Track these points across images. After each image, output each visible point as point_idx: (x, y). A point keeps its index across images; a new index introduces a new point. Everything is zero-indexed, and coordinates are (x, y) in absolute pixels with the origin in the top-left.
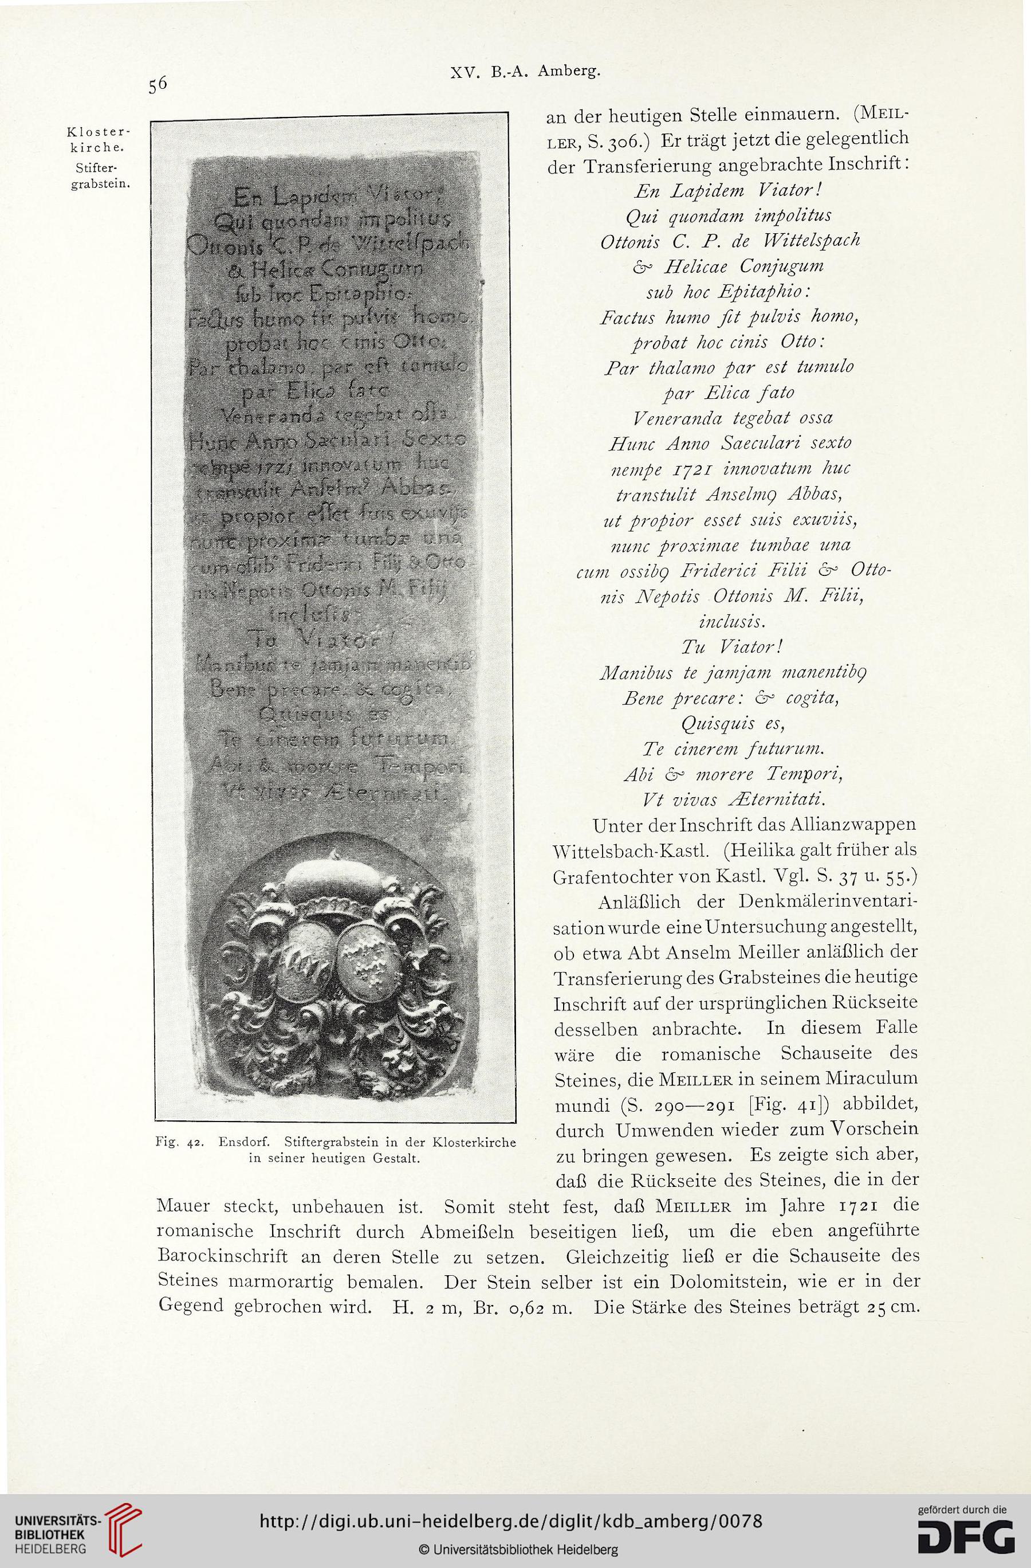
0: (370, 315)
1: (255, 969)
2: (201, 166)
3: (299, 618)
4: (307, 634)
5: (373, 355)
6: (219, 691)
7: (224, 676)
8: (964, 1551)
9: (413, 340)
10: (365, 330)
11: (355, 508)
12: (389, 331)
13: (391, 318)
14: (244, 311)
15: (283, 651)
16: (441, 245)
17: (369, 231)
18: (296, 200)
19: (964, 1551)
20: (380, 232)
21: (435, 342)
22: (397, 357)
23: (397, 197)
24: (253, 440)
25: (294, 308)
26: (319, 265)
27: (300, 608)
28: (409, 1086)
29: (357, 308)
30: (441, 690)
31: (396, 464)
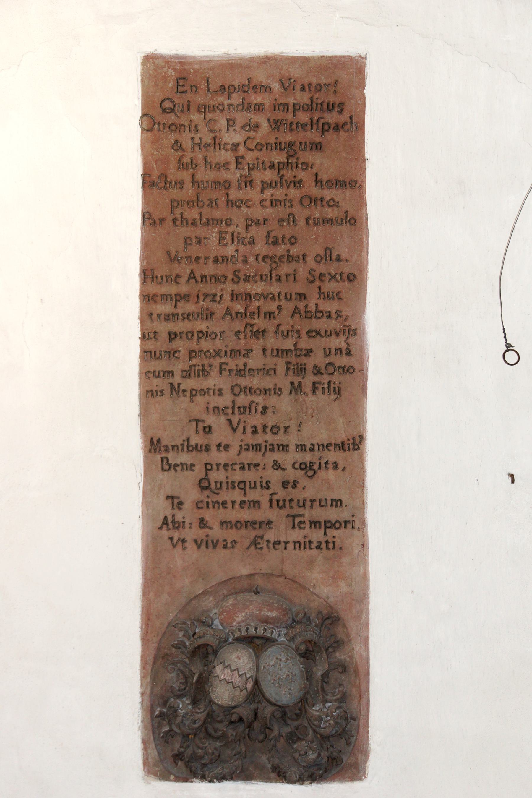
0: (281, 182)
1: (194, 681)
2: (150, 60)
3: (230, 411)
4: (235, 425)
5: (282, 212)
6: (167, 466)
7: (171, 456)
8: (180, 98)
9: (314, 201)
10: (279, 193)
11: (272, 329)
12: (294, 193)
13: (298, 183)
14: (185, 176)
15: (215, 438)
16: (337, 128)
17: (280, 115)
18: (224, 89)
19: (180, 98)
20: (290, 116)
21: (333, 204)
22: (301, 214)
23: (303, 89)
24: (192, 276)
25: (224, 175)
26: (205, 207)
27: (230, 404)
28: (313, 774)
29: (269, 175)
30: (336, 466)
31: (301, 296)
